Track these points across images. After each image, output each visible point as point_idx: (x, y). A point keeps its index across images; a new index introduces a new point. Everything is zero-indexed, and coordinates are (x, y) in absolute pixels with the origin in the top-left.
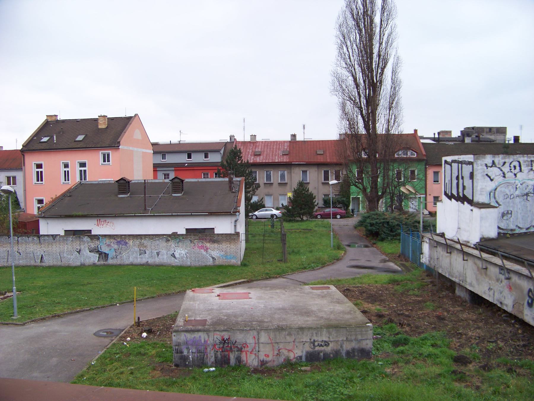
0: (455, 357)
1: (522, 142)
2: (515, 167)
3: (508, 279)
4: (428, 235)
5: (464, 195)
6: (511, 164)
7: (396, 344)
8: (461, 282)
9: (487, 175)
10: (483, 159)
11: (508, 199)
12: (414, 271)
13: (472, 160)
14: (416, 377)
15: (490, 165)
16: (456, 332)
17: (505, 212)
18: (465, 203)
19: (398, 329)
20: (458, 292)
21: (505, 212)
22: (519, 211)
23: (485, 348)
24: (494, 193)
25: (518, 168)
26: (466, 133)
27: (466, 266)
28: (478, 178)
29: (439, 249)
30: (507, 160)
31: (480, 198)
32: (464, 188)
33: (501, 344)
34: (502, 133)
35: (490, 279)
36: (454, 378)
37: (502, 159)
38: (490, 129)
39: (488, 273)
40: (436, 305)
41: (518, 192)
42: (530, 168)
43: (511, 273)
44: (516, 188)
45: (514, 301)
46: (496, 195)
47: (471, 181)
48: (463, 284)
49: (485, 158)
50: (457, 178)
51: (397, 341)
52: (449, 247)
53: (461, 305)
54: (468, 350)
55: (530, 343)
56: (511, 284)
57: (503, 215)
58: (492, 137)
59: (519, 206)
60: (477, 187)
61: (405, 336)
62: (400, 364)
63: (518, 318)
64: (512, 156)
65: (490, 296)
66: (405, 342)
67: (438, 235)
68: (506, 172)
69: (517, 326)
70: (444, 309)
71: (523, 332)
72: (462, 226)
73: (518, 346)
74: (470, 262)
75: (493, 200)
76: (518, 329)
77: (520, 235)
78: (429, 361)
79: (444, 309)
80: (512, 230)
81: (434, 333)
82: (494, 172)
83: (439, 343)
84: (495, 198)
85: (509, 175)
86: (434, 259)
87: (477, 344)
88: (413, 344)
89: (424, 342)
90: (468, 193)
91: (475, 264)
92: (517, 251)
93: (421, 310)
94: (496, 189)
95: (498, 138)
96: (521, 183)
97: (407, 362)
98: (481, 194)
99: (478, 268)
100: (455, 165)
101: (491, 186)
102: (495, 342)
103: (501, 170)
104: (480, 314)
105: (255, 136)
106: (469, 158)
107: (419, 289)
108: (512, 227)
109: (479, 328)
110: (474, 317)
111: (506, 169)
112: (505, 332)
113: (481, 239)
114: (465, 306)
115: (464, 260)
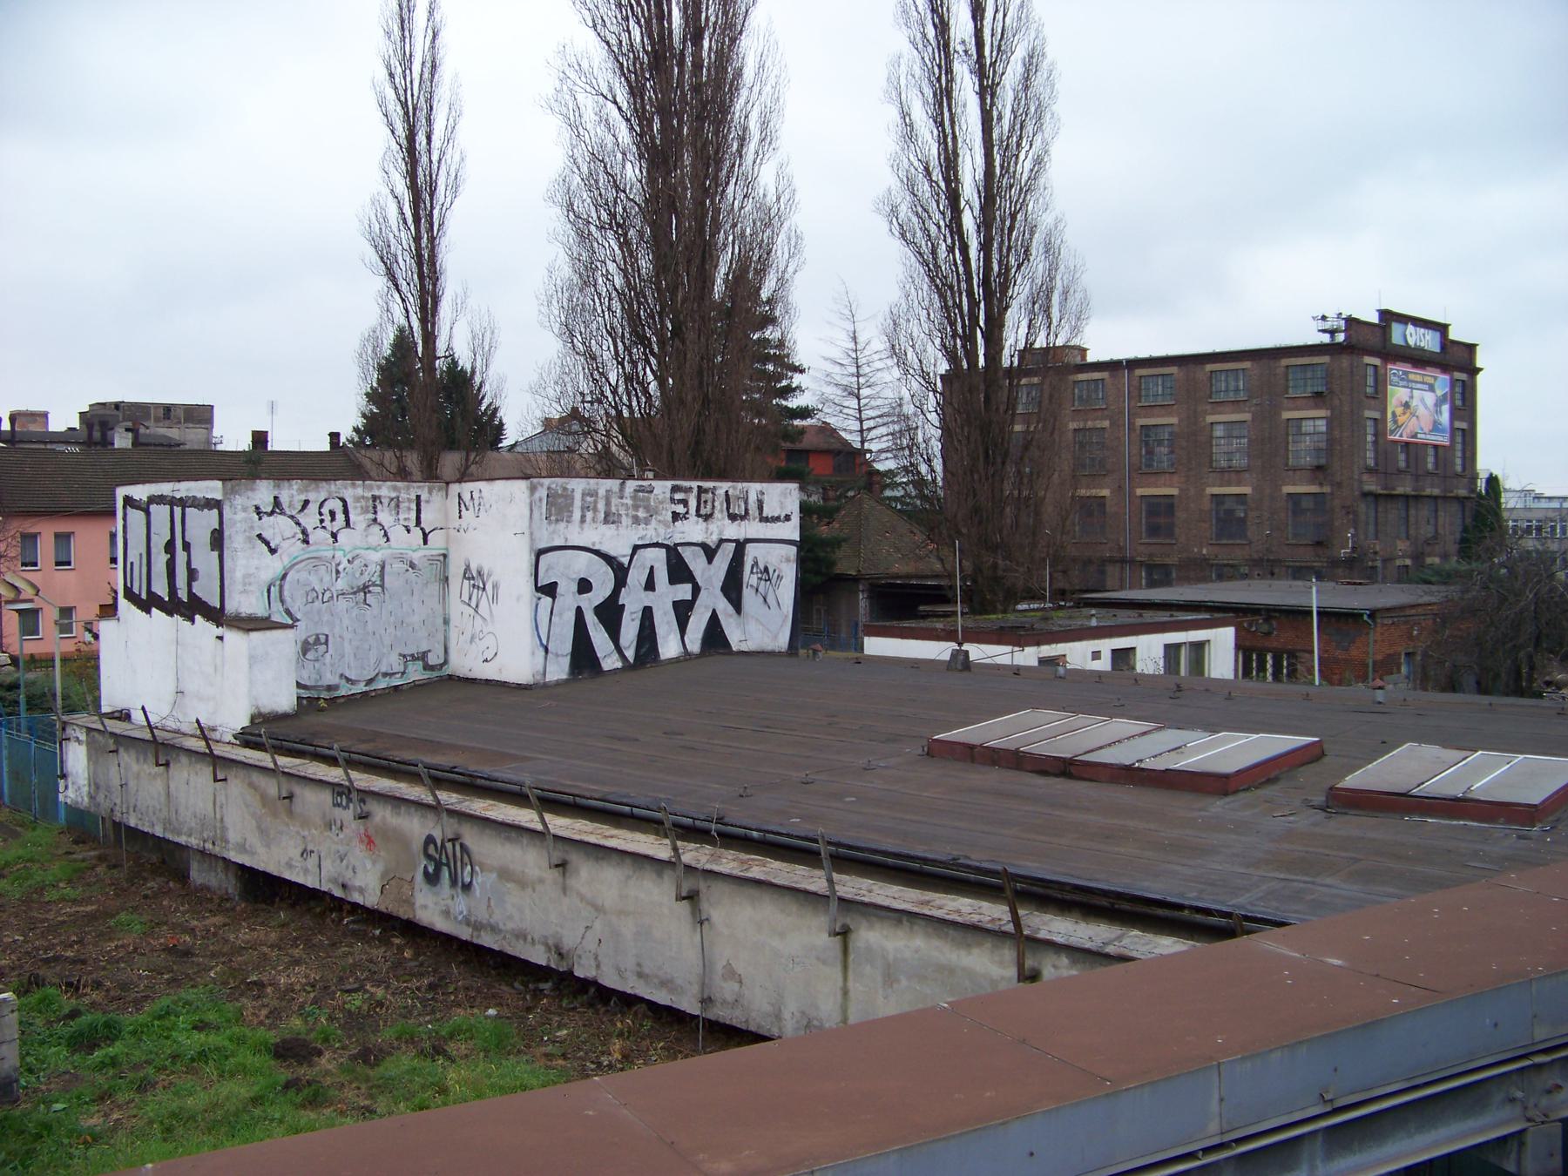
0: (277, 1045)
1: (276, 448)
2: (332, 514)
3: (363, 817)
4: (83, 719)
5: (190, 593)
6: (321, 505)
7: (84, 1042)
8: (209, 846)
9: (259, 536)
10: (250, 493)
11: (317, 604)
12: (29, 834)
13: (219, 497)
14: (192, 1118)
15: (269, 509)
16: (243, 981)
17: (311, 640)
18: (198, 617)
19: (67, 1002)
20: (199, 874)
21: (311, 640)
22: (347, 636)
23: (342, 1009)
24: (281, 587)
25: (340, 517)
26: (100, 420)
27: (221, 798)
28: (235, 545)
29: (127, 757)
30: (312, 496)
31: (243, 602)
32: (192, 575)
33: (380, 993)
34: (200, 422)
35: (305, 823)
36: (299, 1100)
37: (300, 491)
38: (168, 410)
39: (297, 806)
40: (145, 918)
41: (341, 584)
42: (371, 516)
43: (369, 800)
44: (338, 572)
45: (383, 876)
46: (286, 593)
47: (216, 554)
48: (217, 850)
49: (253, 490)
50: (170, 547)
51: (82, 1034)
52: (161, 748)
53: (220, 910)
54: (297, 1022)
55: (444, 977)
56: (371, 832)
57: (306, 647)
58: (174, 433)
59: (346, 622)
60: (234, 571)
61: (97, 1017)
62: (121, 1098)
63: (397, 918)
64: (324, 484)
65: (306, 871)
66: (111, 1032)
67: (111, 716)
68: (310, 530)
69: (397, 941)
70: (174, 927)
71: (416, 955)
72: (190, 686)
73: (418, 989)
74: (236, 786)
75: (276, 606)
76: (400, 949)
77: (351, 699)
78: (210, 1069)
79: (174, 927)
80: (329, 688)
81: (188, 994)
82: (277, 529)
83: (211, 1017)
84: (282, 601)
85: (318, 536)
86: (108, 789)
87: (315, 1002)
88: (134, 1033)
89: (167, 1023)
90: (207, 590)
91: (251, 785)
92: (364, 742)
93: (111, 940)
94: (284, 577)
95: (191, 436)
96: (349, 557)
97: (144, 1087)
98: (245, 591)
99: (264, 798)
100: (160, 513)
101: (274, 566)
102: (361, 988)
103: (298, 524)
104: (283, 925)
105: (265, 434)
106: (211, 489)
107: (69, 881)
108: (330, 678)
109: (297, 962)
110: (273, 935)
111: (310, 519)
112: (371, 961)
113: (253, 718)
114: (233, 909)
115: (216, 780)
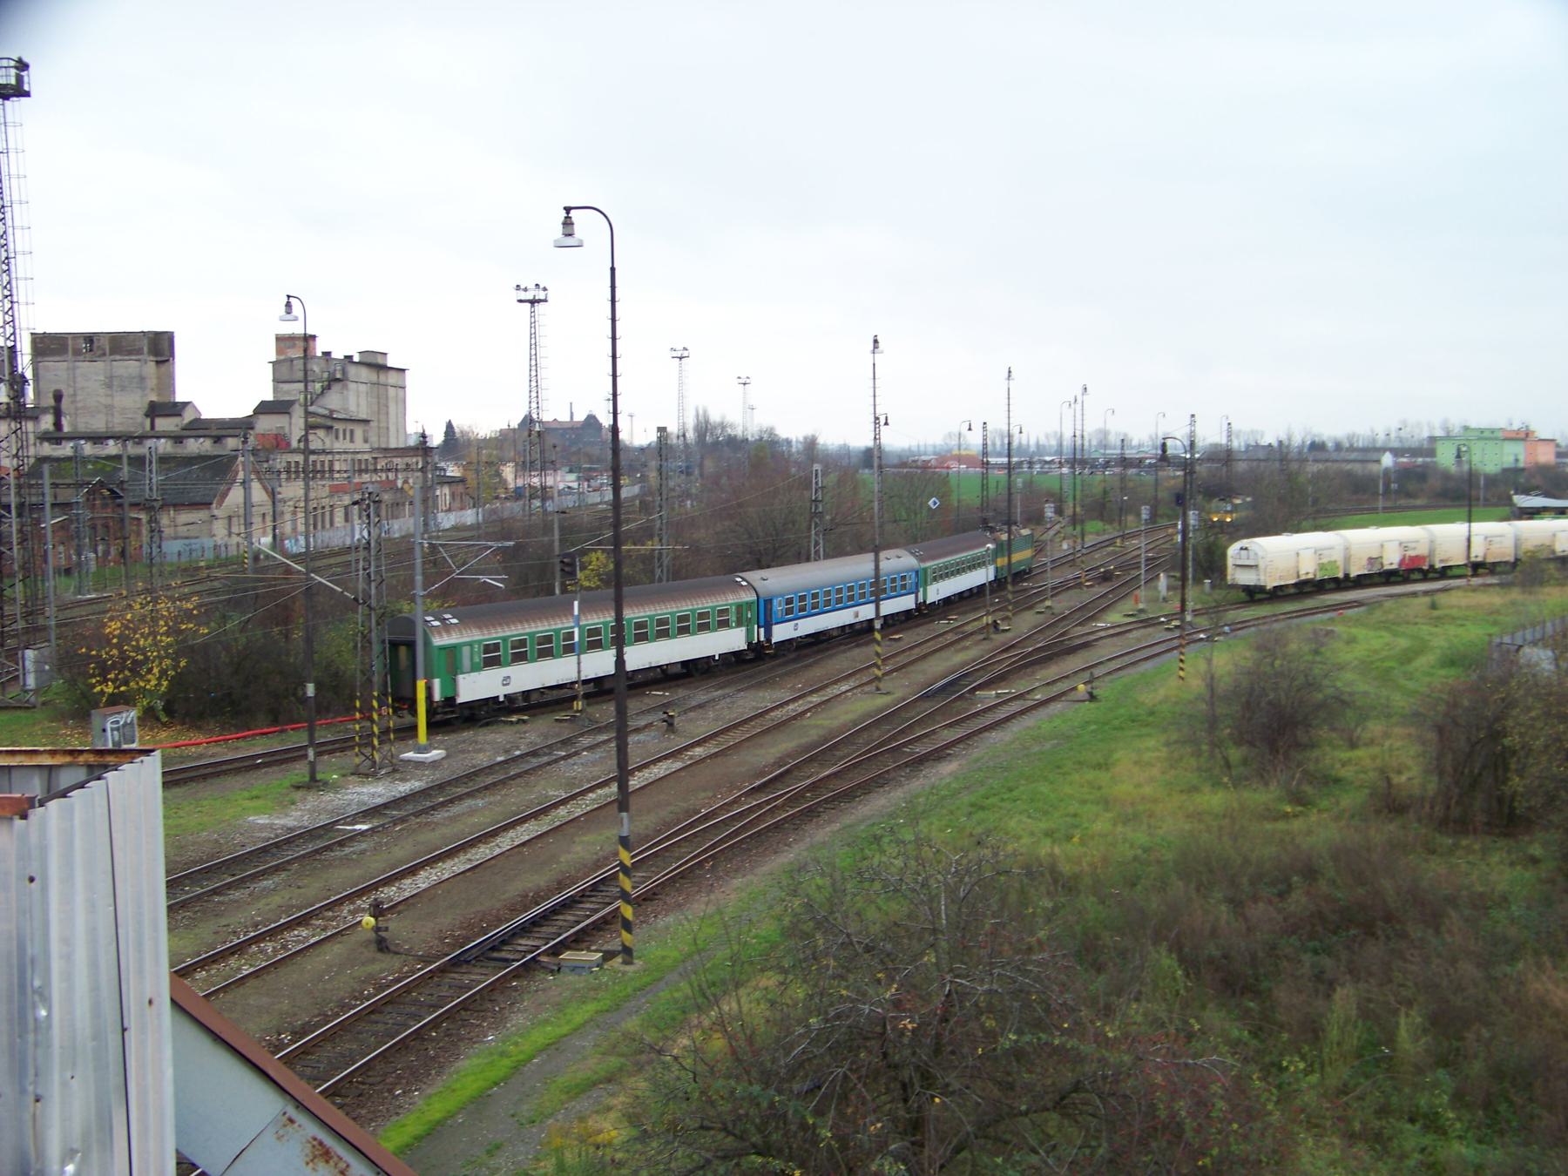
34: (130, 353)
